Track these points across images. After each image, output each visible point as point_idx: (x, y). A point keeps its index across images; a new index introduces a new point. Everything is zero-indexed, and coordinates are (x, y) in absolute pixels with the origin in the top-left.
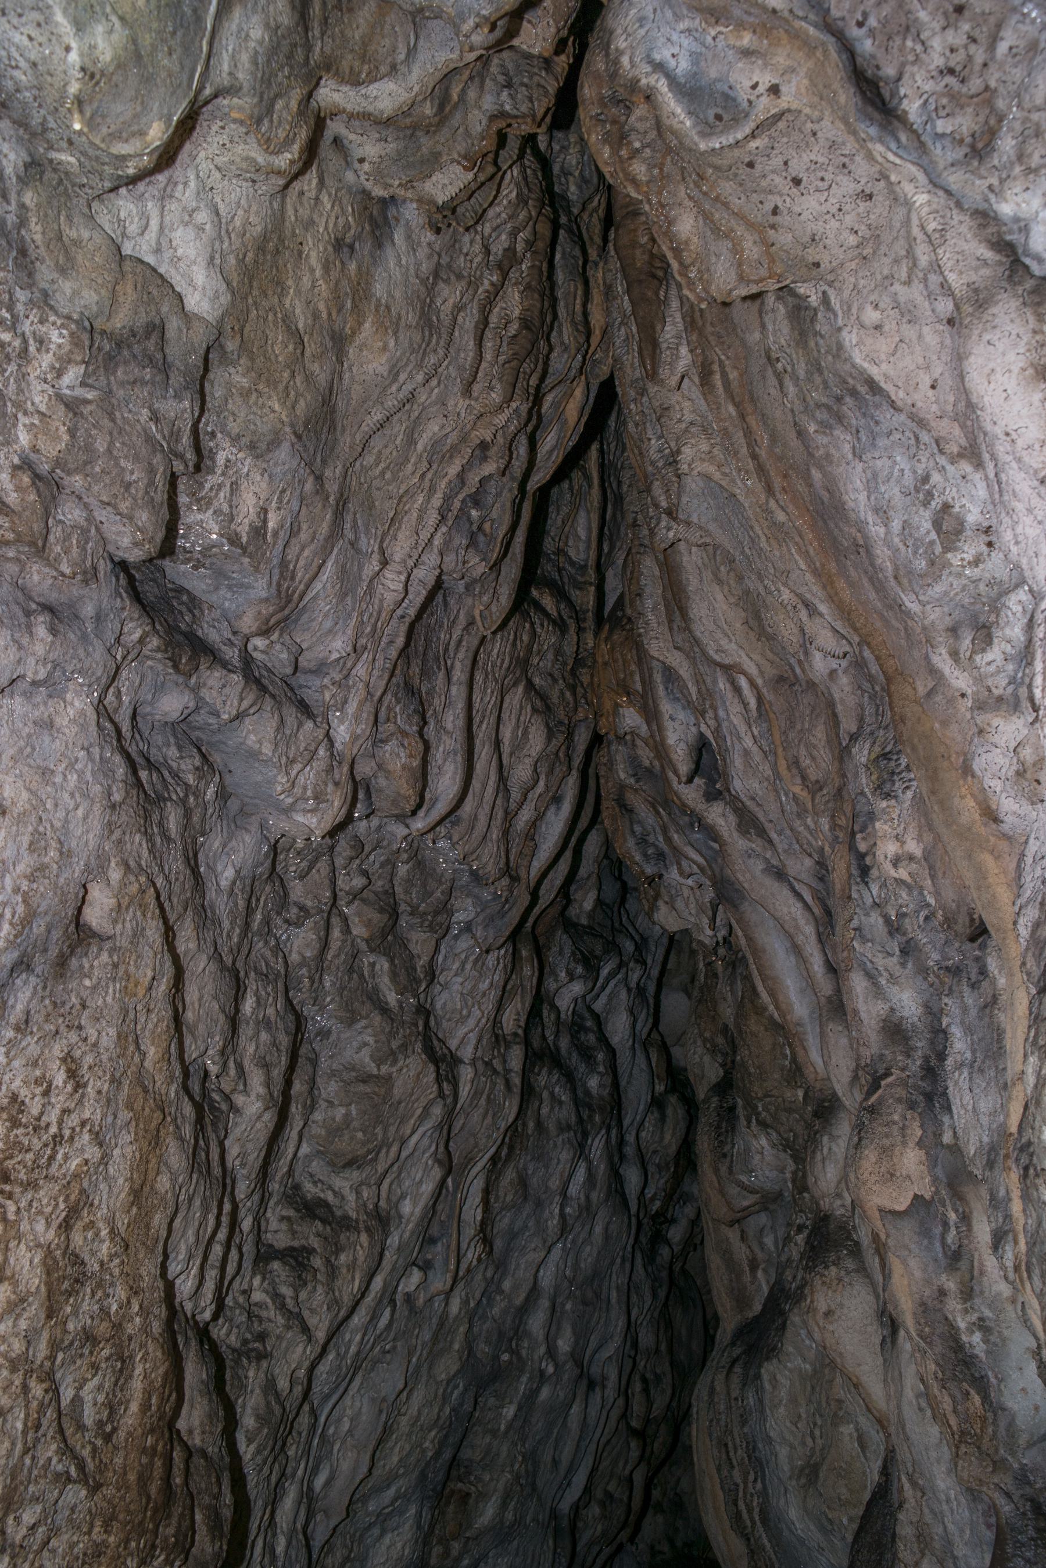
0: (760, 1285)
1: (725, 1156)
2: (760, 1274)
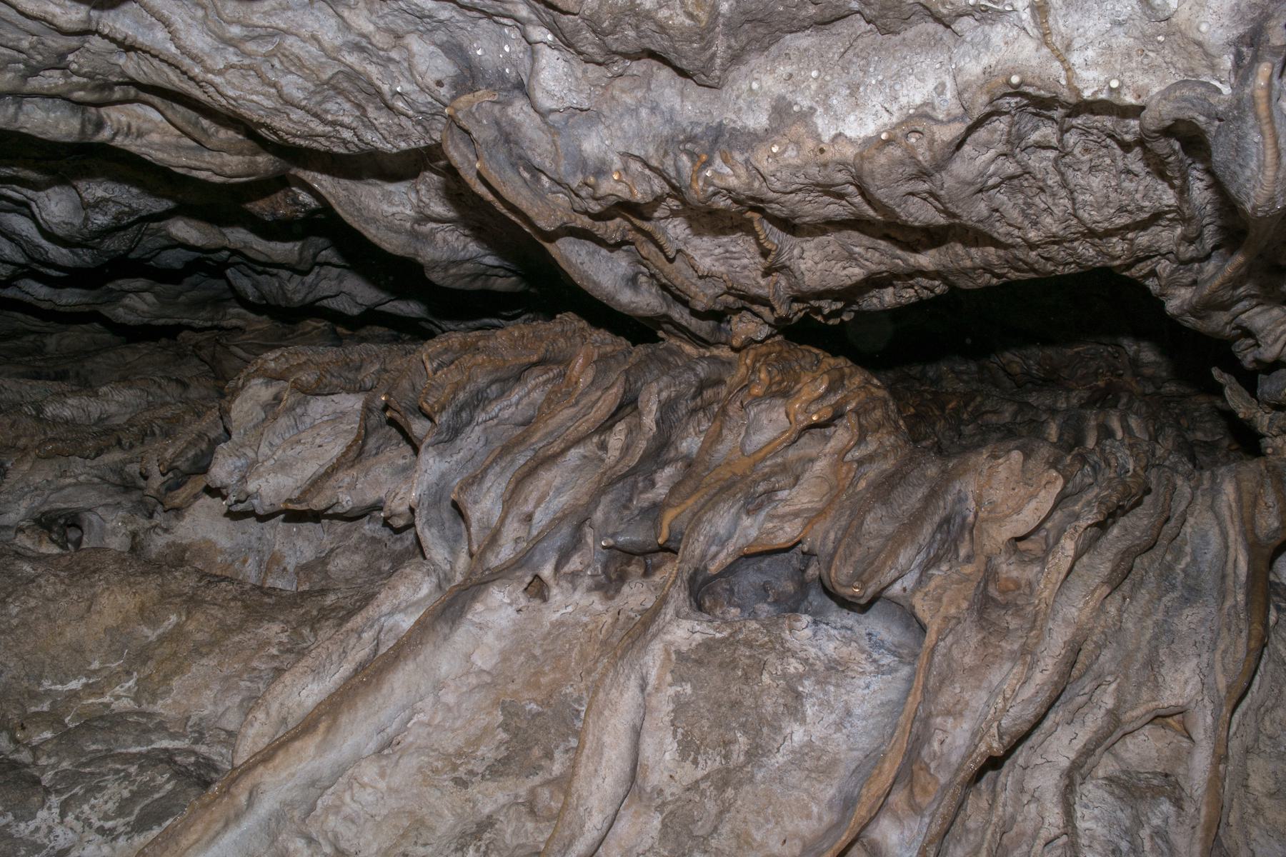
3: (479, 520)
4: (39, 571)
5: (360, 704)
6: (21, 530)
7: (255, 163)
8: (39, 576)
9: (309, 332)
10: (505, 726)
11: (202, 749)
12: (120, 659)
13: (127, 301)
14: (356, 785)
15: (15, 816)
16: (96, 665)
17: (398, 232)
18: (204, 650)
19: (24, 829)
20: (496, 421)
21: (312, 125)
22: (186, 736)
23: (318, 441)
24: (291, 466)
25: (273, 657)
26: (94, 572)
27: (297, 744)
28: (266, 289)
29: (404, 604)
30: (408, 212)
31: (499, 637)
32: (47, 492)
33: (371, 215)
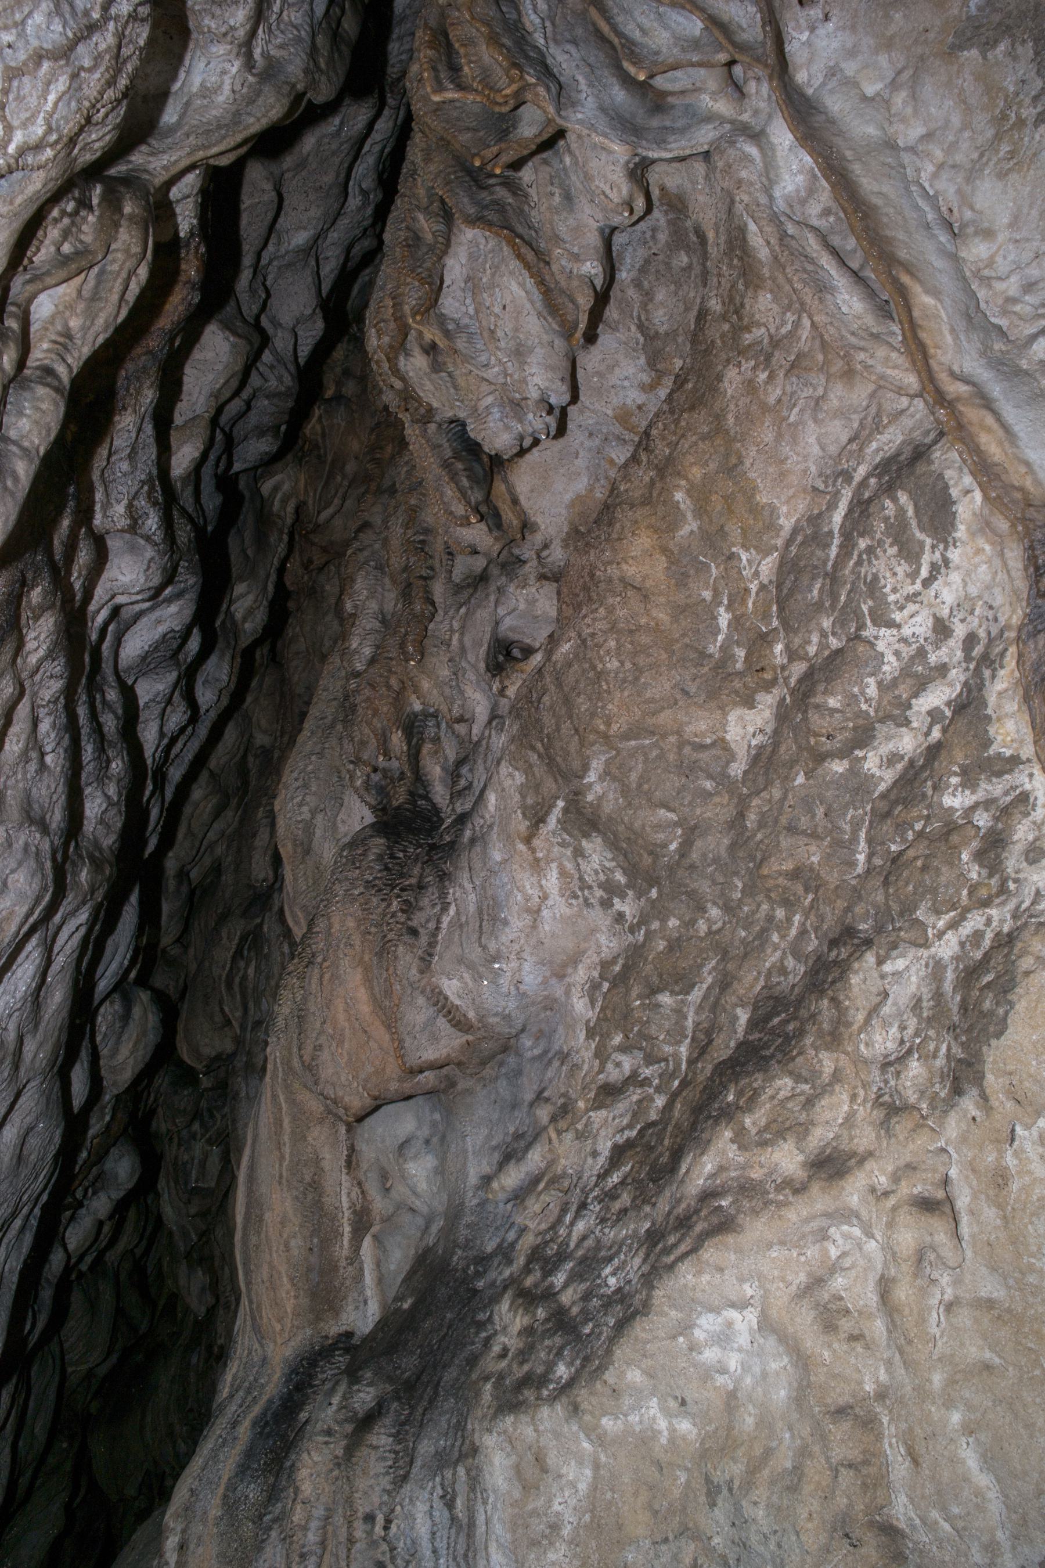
0: (361, 1269)
1: (414, 932)
2: (367, 1242)
3: (683, 50)
4: (573, 634)
5: (888, 233)
6: (502, 692)
7: (131, 218)
8: (580, 635)
9: (323, 428)
10: (990, 44)
11: (862, 471)
12: (708, 567)
13: (238, 616)
14: (986, 272)
15: (872, 675)
16: (707, 595)
17: (259, 93)
18: (734, 460)
19: (891, 666)
20: (548, 24)
21: (103, 46)
22: (838, 492)
23: (497, 309)
24: (520, 345)
25: (771, 377)
26: (592, 575)
27: (916, 313)
28: (267, 420)
29: (764, 179)
30: (234, 70)
31: (852, 53)
32: (464, 664)
33: (229, 116)
